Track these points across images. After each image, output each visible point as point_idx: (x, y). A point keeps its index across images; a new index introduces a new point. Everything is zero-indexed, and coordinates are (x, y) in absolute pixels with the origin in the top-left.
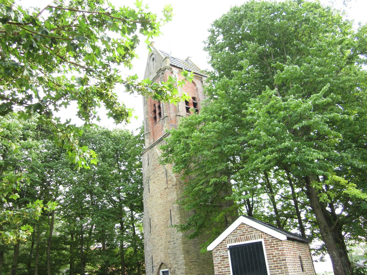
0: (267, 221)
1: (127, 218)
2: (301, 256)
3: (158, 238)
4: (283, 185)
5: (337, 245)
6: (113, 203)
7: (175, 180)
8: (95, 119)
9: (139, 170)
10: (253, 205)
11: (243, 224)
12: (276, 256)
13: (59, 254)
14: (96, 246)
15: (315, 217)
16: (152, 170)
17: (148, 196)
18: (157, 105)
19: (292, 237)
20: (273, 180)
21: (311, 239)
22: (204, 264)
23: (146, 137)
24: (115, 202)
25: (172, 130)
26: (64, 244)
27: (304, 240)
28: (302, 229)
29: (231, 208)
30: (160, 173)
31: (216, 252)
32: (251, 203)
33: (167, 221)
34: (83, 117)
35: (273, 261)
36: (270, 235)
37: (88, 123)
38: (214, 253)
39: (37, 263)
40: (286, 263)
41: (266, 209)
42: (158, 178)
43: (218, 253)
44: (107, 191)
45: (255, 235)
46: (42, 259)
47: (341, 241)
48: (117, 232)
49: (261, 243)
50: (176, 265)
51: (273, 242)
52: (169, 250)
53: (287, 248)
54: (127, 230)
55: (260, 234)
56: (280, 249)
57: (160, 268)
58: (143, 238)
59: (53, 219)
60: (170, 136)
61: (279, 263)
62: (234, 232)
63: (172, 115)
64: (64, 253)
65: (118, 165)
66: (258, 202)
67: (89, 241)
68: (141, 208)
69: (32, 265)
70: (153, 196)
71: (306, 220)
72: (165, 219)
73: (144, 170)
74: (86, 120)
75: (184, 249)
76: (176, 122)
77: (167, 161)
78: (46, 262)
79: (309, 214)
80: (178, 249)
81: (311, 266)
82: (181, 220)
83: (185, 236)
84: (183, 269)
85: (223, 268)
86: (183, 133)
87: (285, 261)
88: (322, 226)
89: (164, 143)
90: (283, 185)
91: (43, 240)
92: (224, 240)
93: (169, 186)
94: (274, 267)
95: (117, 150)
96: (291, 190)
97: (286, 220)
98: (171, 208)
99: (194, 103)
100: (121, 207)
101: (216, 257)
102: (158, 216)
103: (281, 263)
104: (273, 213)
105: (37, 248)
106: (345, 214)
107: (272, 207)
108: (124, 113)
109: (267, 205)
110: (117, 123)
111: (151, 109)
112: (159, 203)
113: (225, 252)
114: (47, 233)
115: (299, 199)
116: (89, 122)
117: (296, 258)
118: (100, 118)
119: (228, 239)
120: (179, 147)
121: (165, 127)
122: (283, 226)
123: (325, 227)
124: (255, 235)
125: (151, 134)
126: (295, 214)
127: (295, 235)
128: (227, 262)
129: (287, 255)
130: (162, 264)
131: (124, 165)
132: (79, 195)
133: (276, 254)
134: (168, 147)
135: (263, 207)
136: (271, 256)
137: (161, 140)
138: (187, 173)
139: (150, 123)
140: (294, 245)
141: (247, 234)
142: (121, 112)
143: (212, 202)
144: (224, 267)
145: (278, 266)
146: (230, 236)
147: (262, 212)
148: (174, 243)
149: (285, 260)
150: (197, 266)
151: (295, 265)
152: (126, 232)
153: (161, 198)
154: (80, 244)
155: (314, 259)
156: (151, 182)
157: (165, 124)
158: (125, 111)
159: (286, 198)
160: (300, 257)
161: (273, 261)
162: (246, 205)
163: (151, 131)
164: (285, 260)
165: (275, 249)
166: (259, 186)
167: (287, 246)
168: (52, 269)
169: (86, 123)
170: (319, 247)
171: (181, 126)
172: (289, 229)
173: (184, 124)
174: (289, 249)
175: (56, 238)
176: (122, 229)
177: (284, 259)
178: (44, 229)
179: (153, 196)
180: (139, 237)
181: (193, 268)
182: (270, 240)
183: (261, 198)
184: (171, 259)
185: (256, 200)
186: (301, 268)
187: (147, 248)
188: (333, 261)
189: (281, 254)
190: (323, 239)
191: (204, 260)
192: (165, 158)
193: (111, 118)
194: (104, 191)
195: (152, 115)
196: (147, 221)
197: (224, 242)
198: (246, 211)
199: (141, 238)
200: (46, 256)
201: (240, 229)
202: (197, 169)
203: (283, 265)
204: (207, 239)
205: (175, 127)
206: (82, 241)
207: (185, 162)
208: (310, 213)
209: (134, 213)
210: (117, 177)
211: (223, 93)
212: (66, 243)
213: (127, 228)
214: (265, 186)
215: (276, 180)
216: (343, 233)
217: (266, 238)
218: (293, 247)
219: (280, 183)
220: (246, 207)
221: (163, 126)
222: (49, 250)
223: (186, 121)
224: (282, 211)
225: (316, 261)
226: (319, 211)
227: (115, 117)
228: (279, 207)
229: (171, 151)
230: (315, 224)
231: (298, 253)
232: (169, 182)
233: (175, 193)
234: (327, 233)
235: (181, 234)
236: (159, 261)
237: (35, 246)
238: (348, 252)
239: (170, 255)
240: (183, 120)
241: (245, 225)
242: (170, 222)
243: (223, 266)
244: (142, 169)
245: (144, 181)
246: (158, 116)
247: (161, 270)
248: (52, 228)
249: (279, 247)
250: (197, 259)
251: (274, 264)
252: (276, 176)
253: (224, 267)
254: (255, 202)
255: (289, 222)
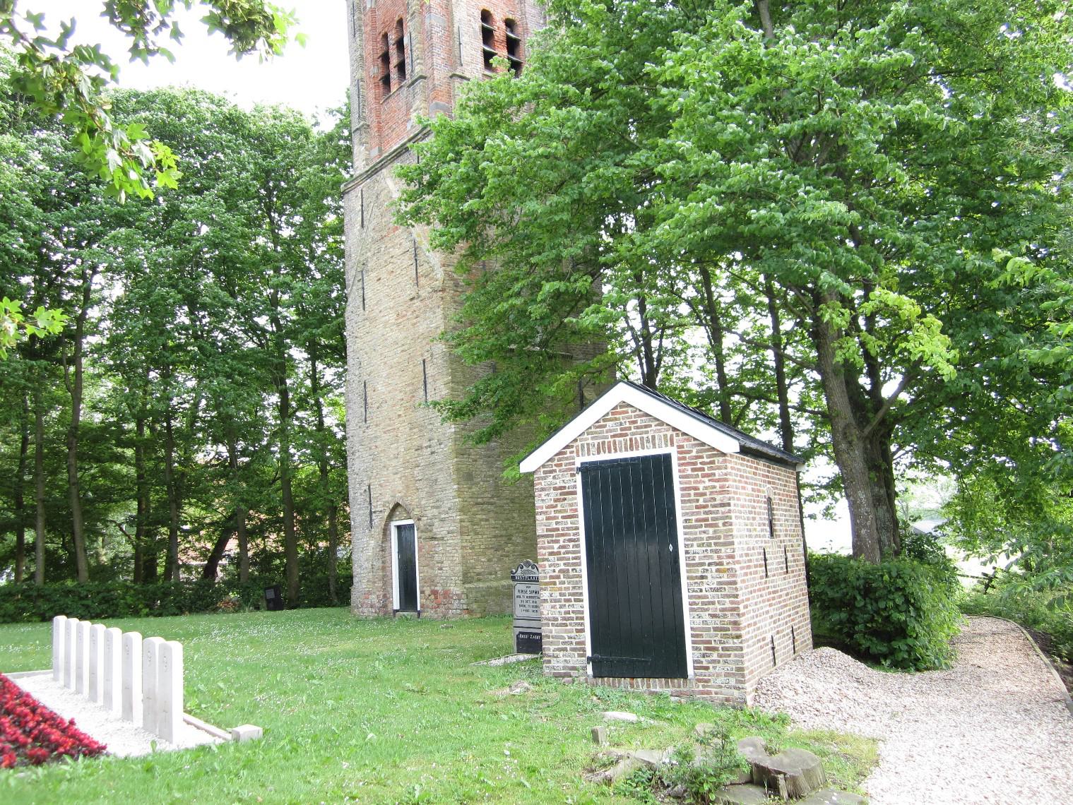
0: (697, 405)
1: (299, 378)
2: (772, 497)
3: (386, 436)
4: (751, 309)
5: (873, 474)
6: (258, 336)
7: (440, 274)
8: (166, 32)
9: (336, 242)
10: (659, 360)
11: (625, 405)
12: (704, 494)
13: (105, 473)
14: (208, 454)
15: (825, 402)
16: (375, 241)
17: (360, 319)
18: (392, 38)
19: (753, 446)
20: (724, 292)
21: (807, 455)
22: (512, 511)
23: (356, 138)
24: (264, 331)
25: (436, 119)
26: (118, 445)
27: (787, 458)
28: (787, 431)
29: (594, 363)
30: (397, 251)
31: (545, 478)
32: (655, 355)
33: (415, 391)
34: (124, 21)
35: (697, 507)
36: (695, 439)
37: (142, 46)
38: (539, 478)
39: (41, 496)
40: (729, 511)
41: (696, 373)
42: (390, 267)
43: (550, 479)
44: (239, 300)
45: (653, 437)
46: (53, 485)
47: (884, 466)
48: (270, 415)
49: (667, 458)
50: (435, 512)
51: (702, 457)
52: (416, 471)
53: (736, 475)
54: (299, 414)
55: (669, 433)
56: (717, 477)
57: (390, 517)
58: (344, 438)
59: (78, 373)
60: (431, 140)
61: (711, 512)
62: (598, 424)
63: (440, 74)
64: (119, 472)
65: (272, 222)
66: (674, 353)
67: (189, 438)
68: (339, 352)
69: (26, 500)
70: (375, 319)
71: (801, 408)
72: (408, 385)
73: (352, 239)
74: (133, 32)
75: (458, 470)
76: (450, 96)
77: (417, 214)
78: (67, 494)
79: (813, 393)
80: (441, 470)
81: (796, 526)
82: (453, 389)
83: (461, 438)
84: (454, 521)
85: (560, 520)
86: (469, 130)
87: (728, 508)
88: (841, 424)
89: (410, 162)
90: (751, 309)
91: (55, 433)
92: (567, 447)
93: (423, 293)
94: (697, 520)
95: (267, 172)
96: (771, 325)
97: (747, 406)
98: (427, 355)
99: (508, 38)
100: (281, 346)
101: (543, 489)
102: (388, 376)
103: (717, 512)
104: (715, 386)
105: (39, 456)
106: (905, 397)
107: (713, 367)
108: (257, 17)
109: (701, 361)
110: (241, 52)
111: (372, 50)
112: (390, 340)
113: (568, 478)
114: (63, 412)
115: (789, 351)
116: (145, 39)
117: (758, 502)
118: (181, 28)
119: (579, 443)
120: (454, 173)
121: (415, 111)
122: (737, 422)
123: (847, 426)
124: (653, 437)
125: (374, 131)
126: (774, 391)
127: (769, 444)
128: (571, 505)
129: (735, 493)
130: (397, 505)
131: (288, 224)
132: (159, 311)
133: (706, 488)
134: (421, 173)
135: (689, 366)
136: (692, 492)
137: (403, 150)
138: (473, 254)
139: (371, 94)
140: (756, 468)
141: (633, 434)
142: (250, 13)
143: (544, 344)
144: (563, 517)
145: (707, 520)
146: (586, 436)
147: (686, 380)
148: (432, 453)
149: (729, 505)
150: (492, 514)
151: (754, 519)
152: (297, 419)
153: (398, 325)
154: (163, 446)
155: (806, 511)
156: (370, 278)
157: (418, 103)
158: (261, 12)
159: (757, 346)
160: (769, 500)
161: (697, 507)
162: (640, 359)
163: (372, 120)
164: (729, 505)
165: (704, 476)
166: (684, 309)
167: (739, 470)
168: (88, 511)
169: (136, 46)
170: (825, 481)
171: (463, 107)
172: (751, 430)
173: (471, 104)
174: (741, 476)
175: (92, 429)
176: (284, 410)
177: (726, 501)
178: (56, 401)
179: (375, 319)
180: (334, 435)
181: (482, 520)
182: (695, 450)
183: (685, 342)
184: (423, 494)
185: (670, 346)
186: (768, 529)
187: (357, 462)
188: (855, 516)
189: (718, 489)
190: (838, 460)
191: (513, 501)
192: (411, 205)
193: (219, 35)
194: (231, 300)
195: (375, 70)
196: (357, 387)
197: (568, 450)
198: (641, 376)
199: (339, 436)
200: (65, 476)
201: (616, 419)
202: (507, 245)
203: (721, 518)
204: (525, 444)
205: (448, 111)
206: (170, 439)
207: (470, 223)
208: (815, 389)
209: (320, 366)
210: (267, 259)
211: (600, 12)
212: (121, 444)
213: (301, 407)
214: (701, 308)
215: (732, 292)
216: (893, 448)
217: (683, 447)
218: (755, 474)
219: (743, 301)
220: (641, 364)
221: (408, 110)
222: (72, 461)
223: (478, 93)
224: (738, 383)
225: (812, 517)
226: (837, 385)
227: (230, 31)
228: (731, 369)
229: (432, 186)
230: (825, 418)
231: (767, 490)
232: (422, 281)
233: (439, 312)
234: (850, 443)
235: (450, 428)
236: (388, 498)
237: (31, 449)
238: (896, 494)
239: (418, 485)
240: (470, 90)
241: (630, 409)
242: (422, 393)
243: (560, 515)
244: (344, 238)
245: (349, 277)
246: (394, 75)
247: (394, 524)
248: (77, 399)
249: (717, 472)
250: (492, 497)
251: (698, 513)
252: (735, 280)
253: (563, 517)
254: (666, 352)
255: (755, 412)
